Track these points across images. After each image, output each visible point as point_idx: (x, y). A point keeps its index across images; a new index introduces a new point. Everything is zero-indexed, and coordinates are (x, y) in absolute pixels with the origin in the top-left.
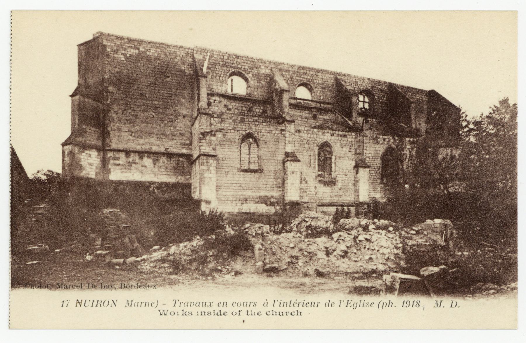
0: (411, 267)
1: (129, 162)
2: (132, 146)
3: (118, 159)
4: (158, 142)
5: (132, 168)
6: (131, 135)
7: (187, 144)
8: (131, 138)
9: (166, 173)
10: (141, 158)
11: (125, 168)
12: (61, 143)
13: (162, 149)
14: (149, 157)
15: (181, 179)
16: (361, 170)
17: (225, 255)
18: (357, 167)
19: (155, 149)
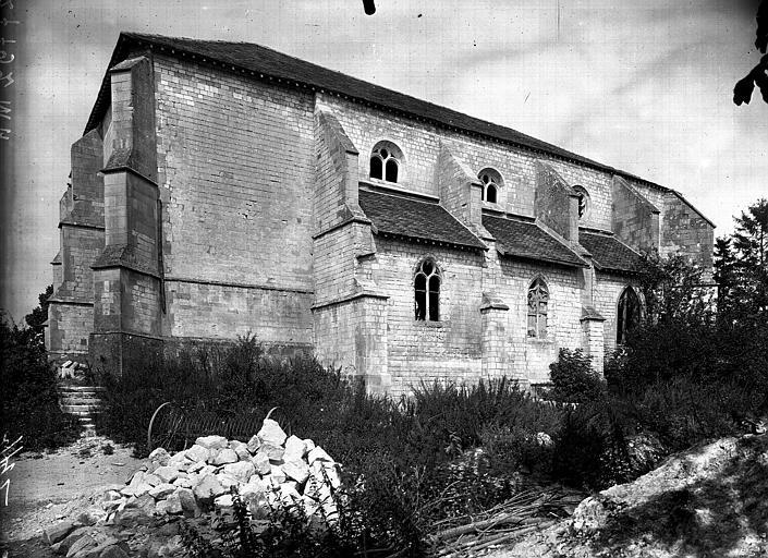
0: (748, 510)
1: (207, 303)
2: (209, 274)
3: (188, 297)
4: (255, 266)
5: (211, 313)
6: (208, 252)
7: (305, 273)
8: (208, 256)
9: (270, 324)
10: (227, 296)
11: (200, 314)
12: (124, 31)
13: (263, 281)
14: (241, 295)
15: (80, 403)
16: (592, 324)
17: (649, 537)
18: (585, 320)
19: (250, 279)
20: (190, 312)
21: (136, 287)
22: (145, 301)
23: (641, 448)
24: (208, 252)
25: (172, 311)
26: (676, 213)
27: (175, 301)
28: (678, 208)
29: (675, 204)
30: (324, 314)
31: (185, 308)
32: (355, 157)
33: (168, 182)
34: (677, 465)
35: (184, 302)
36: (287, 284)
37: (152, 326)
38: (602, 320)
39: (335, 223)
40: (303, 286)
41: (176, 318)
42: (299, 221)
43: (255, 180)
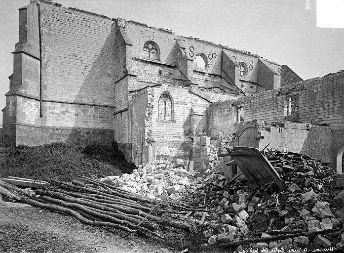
3: (54, 108)
13: (91, 102)
20: (55, 115)
21: (26, 104)
22: (31, 110)
23: (227, 218)
24: (64, 89)
25: (46, 115)
26: (287, 75)
27: (48, 110)
28: (288, 73)
29: (287, 71)
30: (119, 115)
31: (52, 113)
32: (131, 47)
33: (46, 58)
34: (211, 151)
35: (52, 111)
36: (102, 103)
37: (35, 121)
38: (240, 80)
39: (122, 76)
40: (111, 104)
41: (48, 118)
42: (109, 76)
43: (87, 58)
